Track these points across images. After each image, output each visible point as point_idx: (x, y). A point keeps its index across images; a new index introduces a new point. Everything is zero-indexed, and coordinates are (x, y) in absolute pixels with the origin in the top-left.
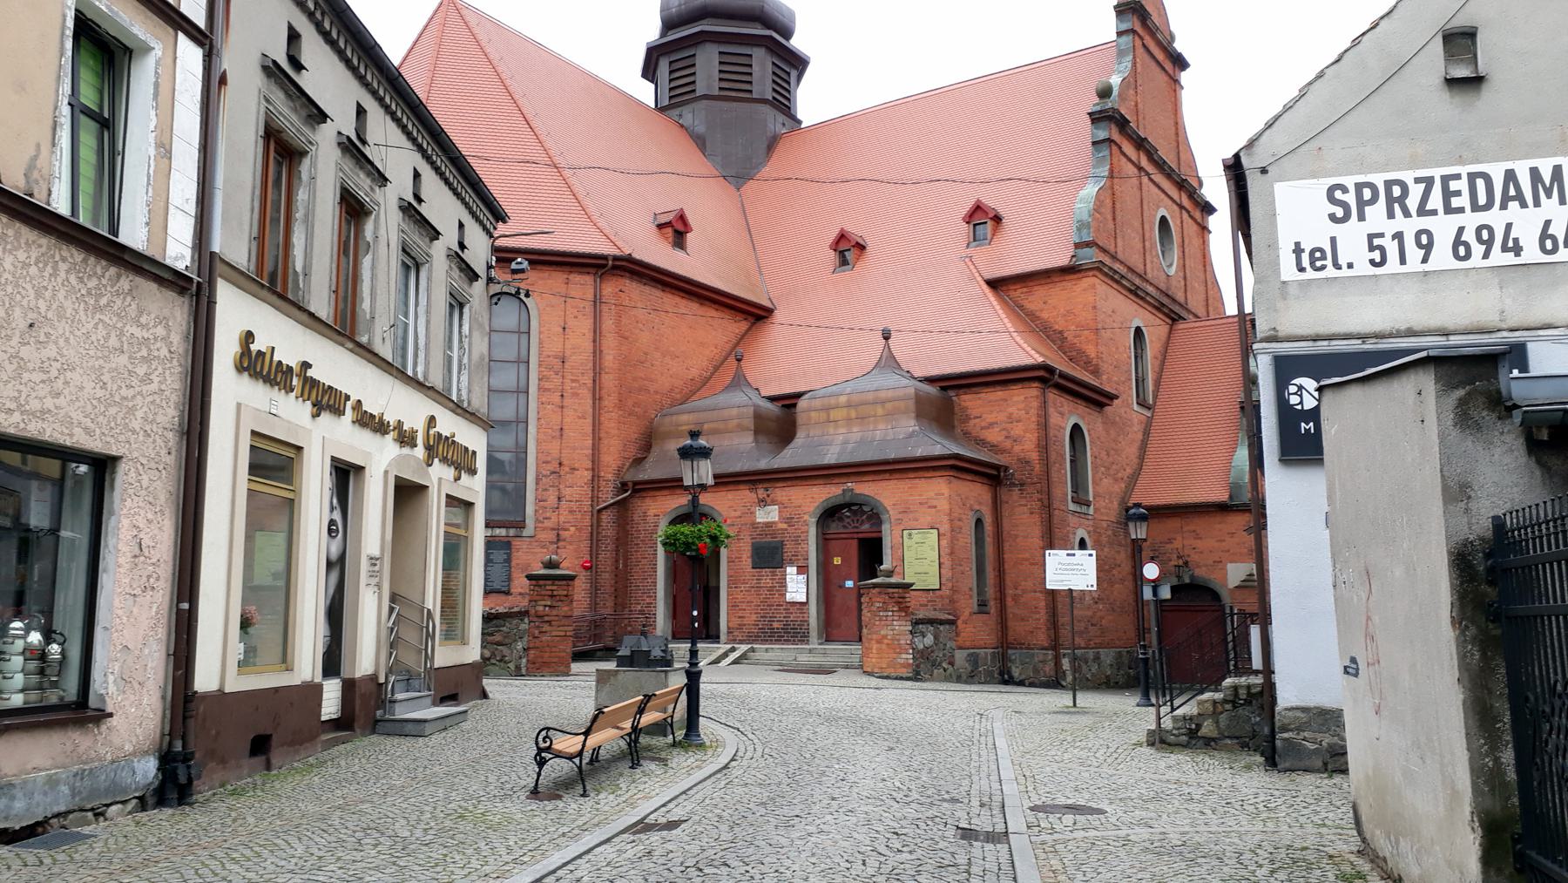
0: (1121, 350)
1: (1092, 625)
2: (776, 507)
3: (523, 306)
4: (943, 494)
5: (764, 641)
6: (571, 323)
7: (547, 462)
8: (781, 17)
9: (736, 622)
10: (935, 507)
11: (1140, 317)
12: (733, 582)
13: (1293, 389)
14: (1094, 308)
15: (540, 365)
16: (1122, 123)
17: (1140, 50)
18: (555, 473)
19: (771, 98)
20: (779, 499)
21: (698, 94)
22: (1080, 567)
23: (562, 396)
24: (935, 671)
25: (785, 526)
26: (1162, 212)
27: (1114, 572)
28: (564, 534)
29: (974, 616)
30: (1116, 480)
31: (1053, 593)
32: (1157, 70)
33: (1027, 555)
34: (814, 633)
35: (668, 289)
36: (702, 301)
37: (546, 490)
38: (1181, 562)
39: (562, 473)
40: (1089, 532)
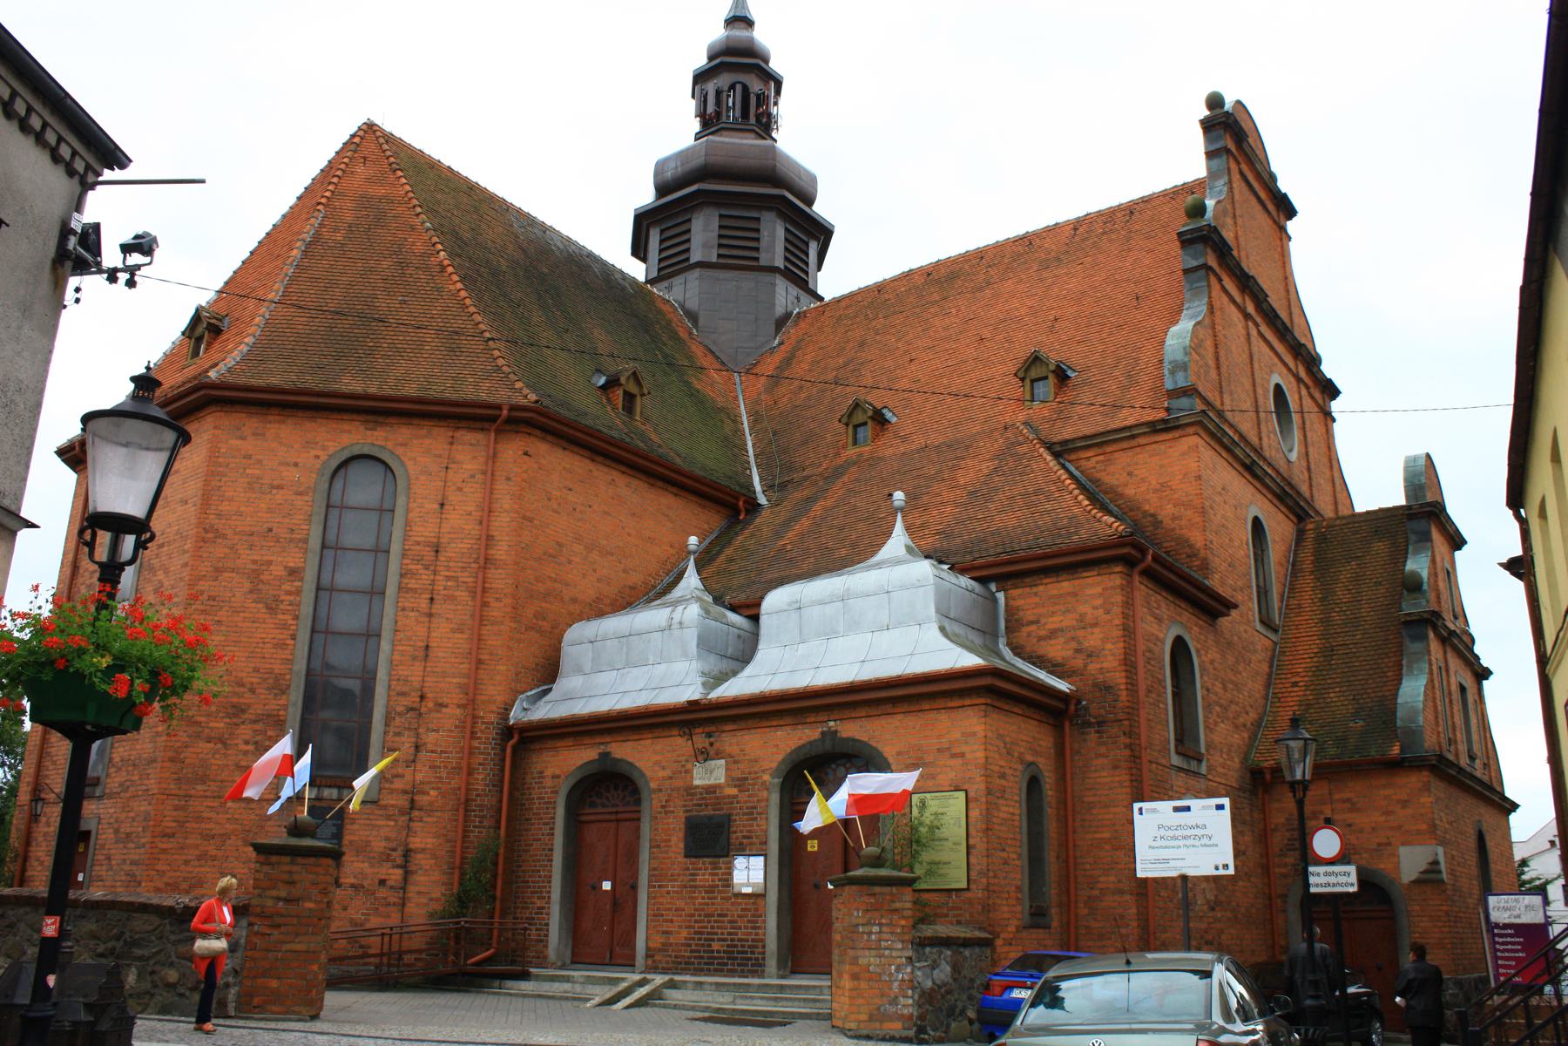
0: (1236, 544)
2: (723, 761)
3: (390, 475)
4: (974, 734)
5: (698, 971)
6: (453, 497)
7: (403, 694)
8: (797, 179)
9: (658, 941)
10: (963, 755)
11: (1258, 506)
12: (656, 876)
14: (1199, 478)
15: (404, 556)
16: (1223, 250)
17: (1236, 177)
18: (412, 709)
19: (782, 268)
20: (728, 749)
21: (692, 261)
22: (1199, 832)
23: (432, 599)
24: (954, 1025)
25: (734, 791)
26: (1276, 379)
28: (422, 799)
29: (1024, 934)
30: (1236, 727)
31: (1146, 887)
32: (1258, 208)
33: (1106, 835)
34: (771, 964)
35: (600, 459)
36: (651, 481)
37: (398, 734)
39: (423, 710)
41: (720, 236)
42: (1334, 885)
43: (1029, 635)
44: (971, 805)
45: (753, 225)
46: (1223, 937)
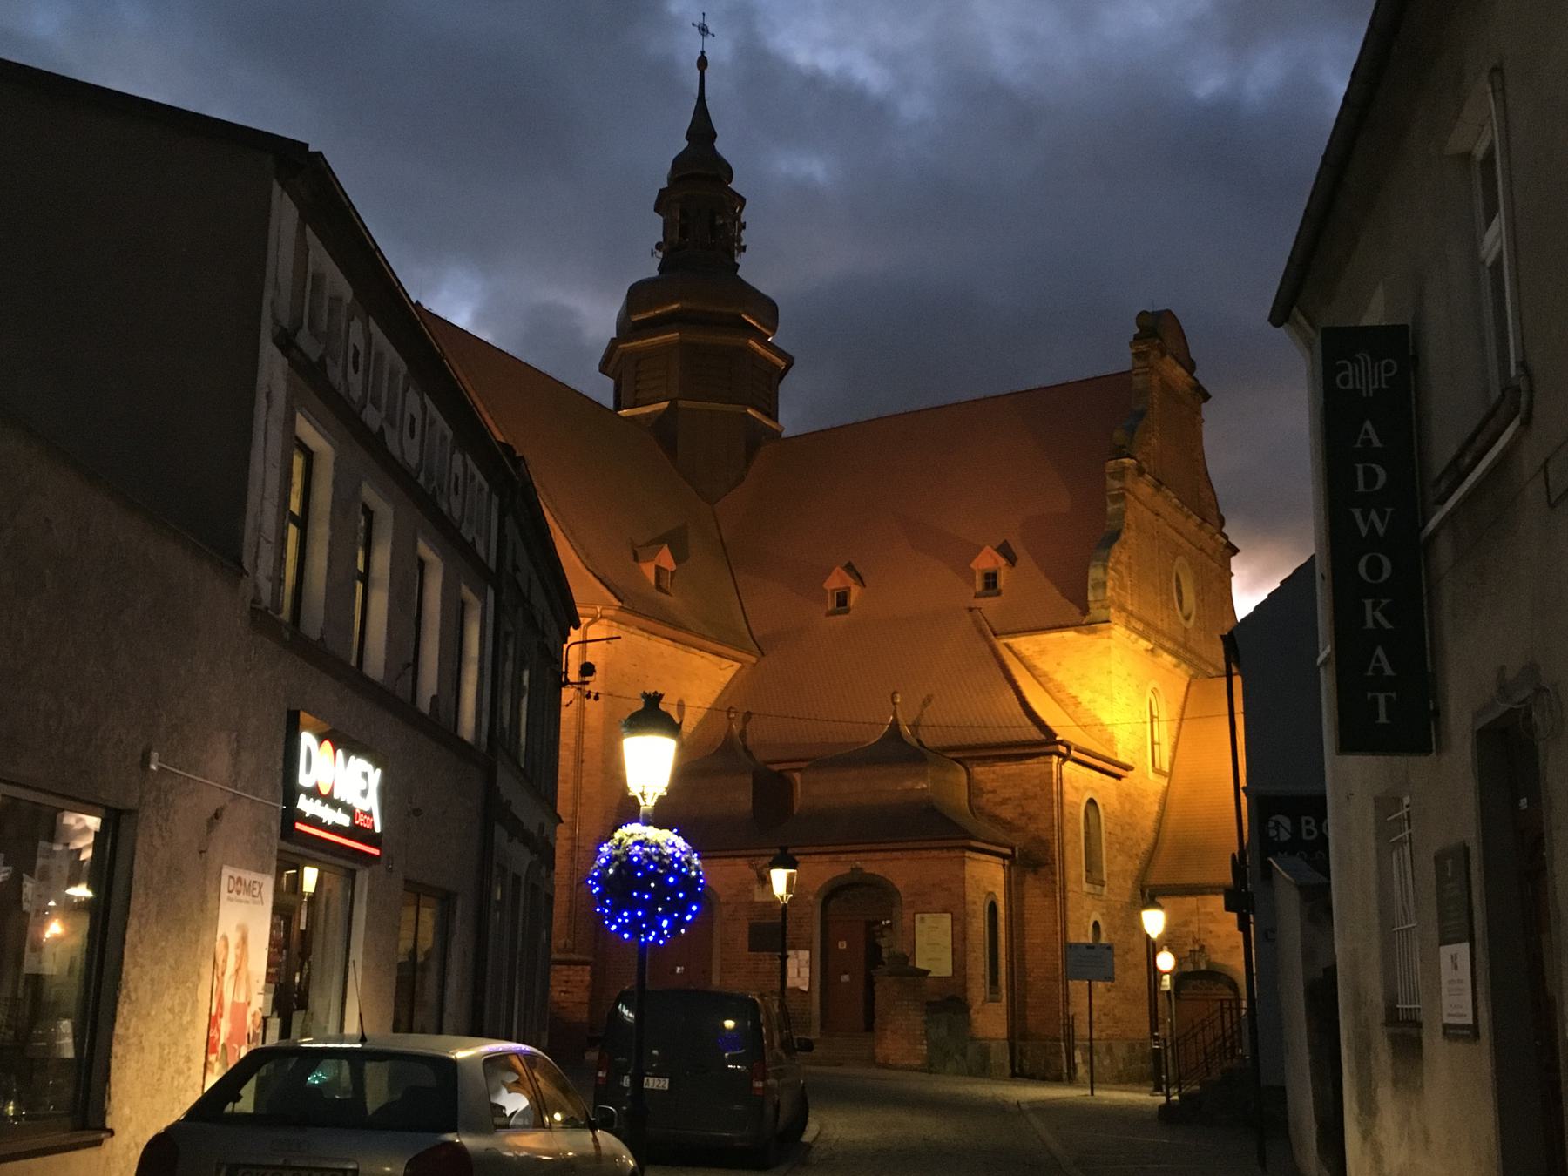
1: (1105, 1014)
13: (1272, 824)
27: (1128, 957)
30: (1131, 857)
38: (1197, 948)
40: (1103, 914)
43: (988, 800)
44: (955, 922)
46: (1116, 1011)
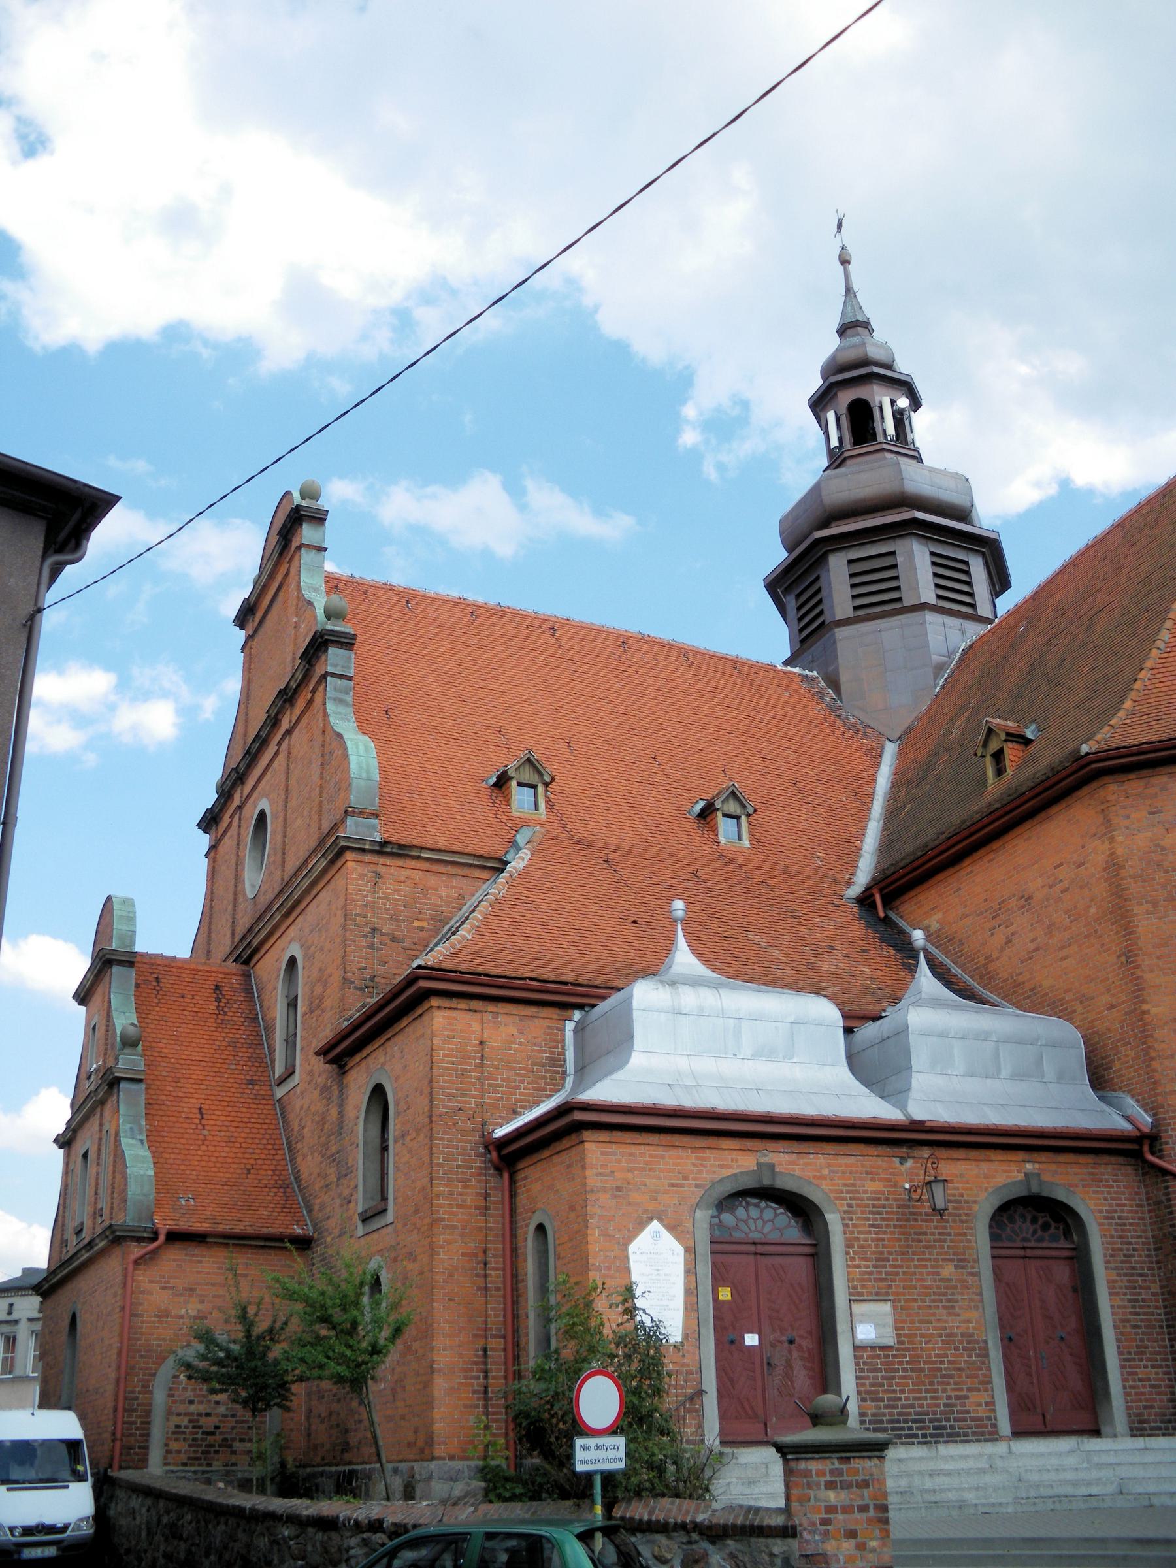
41: (853, 586)
42: (604, 1461)
45: (888, 561)
